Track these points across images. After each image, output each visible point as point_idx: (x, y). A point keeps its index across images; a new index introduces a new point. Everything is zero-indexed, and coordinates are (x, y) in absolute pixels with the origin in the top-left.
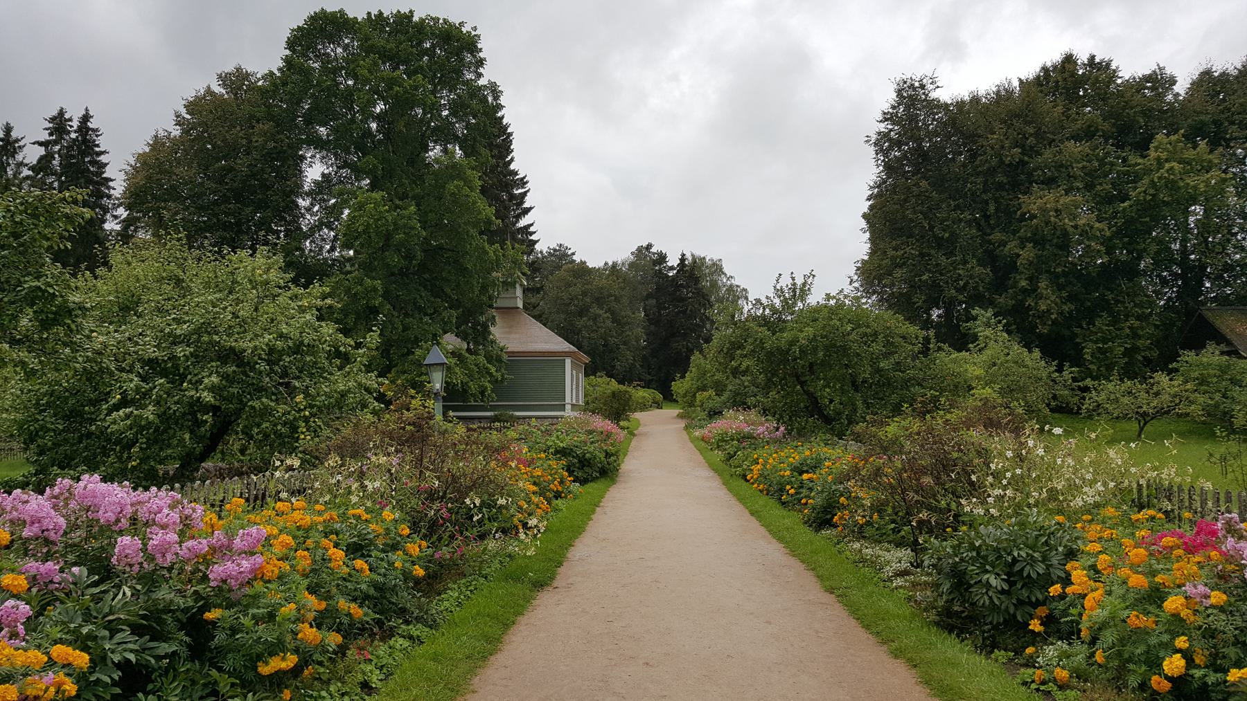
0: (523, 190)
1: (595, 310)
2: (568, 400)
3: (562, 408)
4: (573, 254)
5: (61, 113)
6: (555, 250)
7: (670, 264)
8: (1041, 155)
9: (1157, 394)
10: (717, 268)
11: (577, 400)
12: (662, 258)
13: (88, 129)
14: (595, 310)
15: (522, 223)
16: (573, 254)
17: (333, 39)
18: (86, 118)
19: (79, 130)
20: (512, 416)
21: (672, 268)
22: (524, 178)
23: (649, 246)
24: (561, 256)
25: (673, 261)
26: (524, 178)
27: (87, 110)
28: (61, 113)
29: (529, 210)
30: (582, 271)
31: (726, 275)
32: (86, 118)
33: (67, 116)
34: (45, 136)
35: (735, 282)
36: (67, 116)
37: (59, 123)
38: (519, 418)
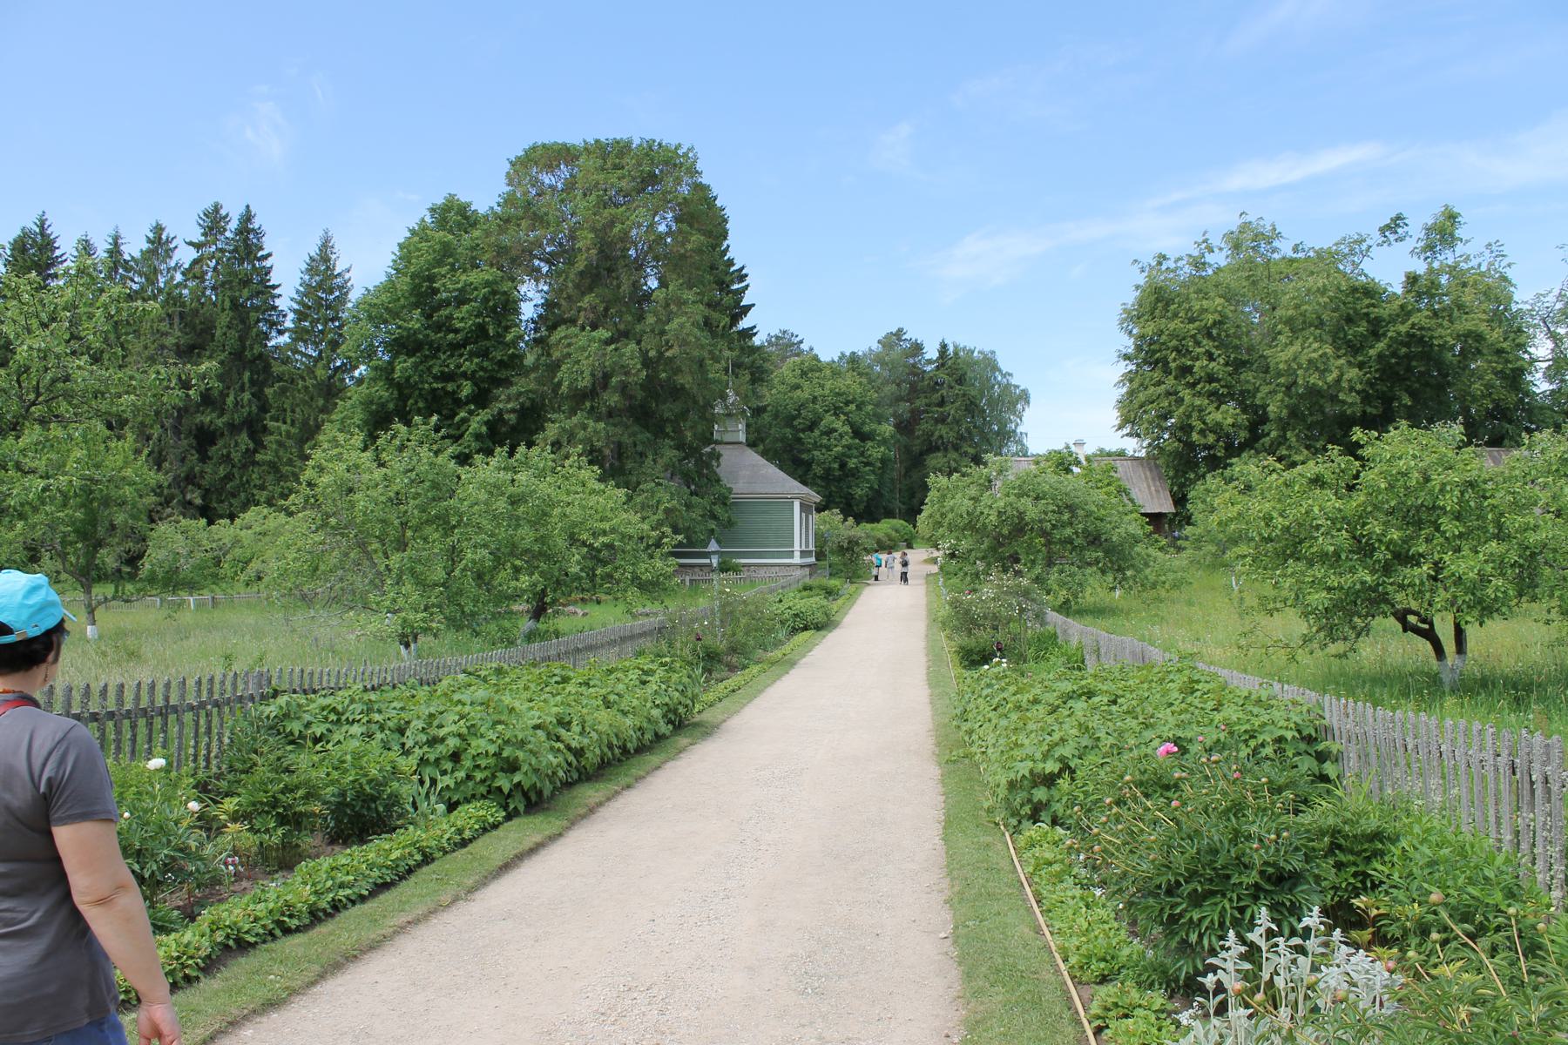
0: (743, 284)
1: (828, 420)
2: (797, 547)
3: (791, 554)
4: (801, 342)
5: (217, 208)
6: (777, 337)
7: (927, 357)
8: (765, 650)
9: (974, 591)
10: (990, 363)
11: (807, 546)
12: (917, 348)
13: (249, 231)
14: (828, 420)
15: (744, 324)
16: (801, 342)
17: (550, 167)
18: (247, 217)
19: (239, 232)
20: (737, 565)
21: (930, 362)
22: (743, 268)
23: (899, 333)
24: (786, 345)
25: (932, 352)
26: (743, 268)
27: (248, 207)
28: (217, 208)
29: (749, 307)
30: (811, 368)
31: (1000, 371)
32: (247, 217)
33: (223, 212)
34: (197, 237)
35: (1014, 381)
36: (223, 212)
37: (214, 221)
38: (744, 565)
